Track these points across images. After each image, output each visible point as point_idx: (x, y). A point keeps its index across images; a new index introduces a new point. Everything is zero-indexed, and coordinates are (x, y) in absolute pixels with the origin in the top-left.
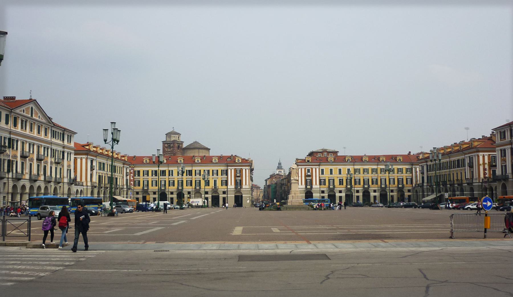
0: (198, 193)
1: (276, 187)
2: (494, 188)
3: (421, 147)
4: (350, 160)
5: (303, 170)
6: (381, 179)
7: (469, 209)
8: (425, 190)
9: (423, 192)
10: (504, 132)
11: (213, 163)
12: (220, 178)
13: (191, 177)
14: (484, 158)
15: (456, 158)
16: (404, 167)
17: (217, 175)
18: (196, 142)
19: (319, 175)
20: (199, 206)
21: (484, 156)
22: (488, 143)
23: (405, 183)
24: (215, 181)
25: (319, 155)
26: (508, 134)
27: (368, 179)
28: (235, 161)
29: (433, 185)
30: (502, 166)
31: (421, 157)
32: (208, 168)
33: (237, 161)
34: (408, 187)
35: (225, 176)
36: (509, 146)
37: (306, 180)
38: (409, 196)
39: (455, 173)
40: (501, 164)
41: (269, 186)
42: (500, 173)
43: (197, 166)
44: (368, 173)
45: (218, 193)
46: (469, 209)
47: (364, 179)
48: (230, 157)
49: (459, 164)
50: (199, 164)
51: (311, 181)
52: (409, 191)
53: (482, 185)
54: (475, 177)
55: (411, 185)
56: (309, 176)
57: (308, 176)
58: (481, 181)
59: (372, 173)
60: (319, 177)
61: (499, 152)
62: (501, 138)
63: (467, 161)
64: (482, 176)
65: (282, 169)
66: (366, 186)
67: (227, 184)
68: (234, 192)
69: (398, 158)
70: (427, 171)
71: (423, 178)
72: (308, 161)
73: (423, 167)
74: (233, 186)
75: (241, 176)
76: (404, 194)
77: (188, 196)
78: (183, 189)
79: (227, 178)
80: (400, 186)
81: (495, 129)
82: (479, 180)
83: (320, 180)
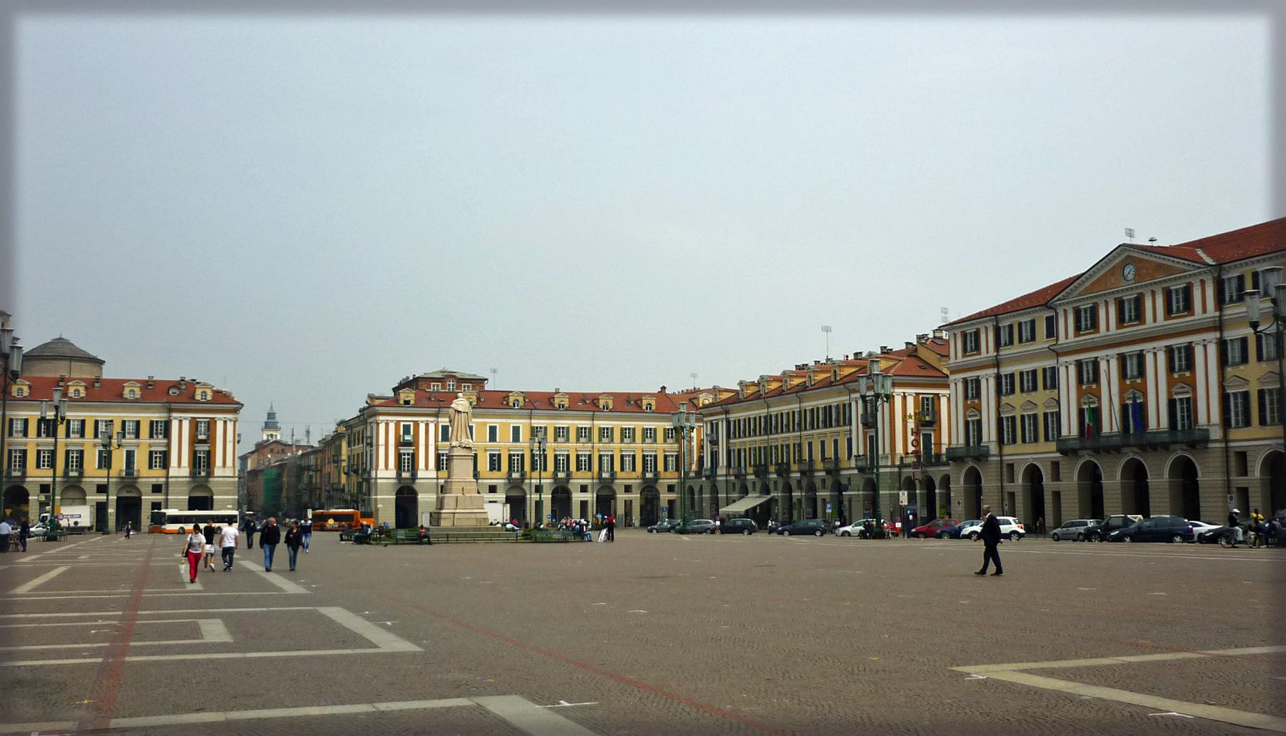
0: (74, 490)
1: (280, 476)
2: (937, 483)
3: (694, 376)
4: (521, 404)
5: (392, 426)
6: (600, 457)
7: (1014, 538)
8: (722, 487)
9: (714, 490)
10: (977, 334)
11: (126, 401)
12: (143, 447)
13: (52, 440)
14: (905, 401)
15: (822, 403)
16: (661, 426)
17: (137, 436)
18: (60, 340)
19: (436, 441)
20: (83, 529)
21: (904, 397)
22: (919, 361)
23: (660, 467)
24: (130, 455)
25: (435, 387)
26: (987, 340)
27: (568, 456)
28: (193, 397)
29: (746, 474)
30: (967, 424)
31: (705, 399)
32: (103, 416)
33: (198, 397)
34: (669, 477)
35: (161, 440)
36: (993, 371)
37: (399, 457)
38: (671, 502)
39: (818, 441)
40: (965, 416)
41: (254, 473)
42: (962, 441)
43: (77, 409)
44: (568, 440)
45: (209, 490)
46: (1014, 538)
47: (556, 456)
48: (176, 385)
49: (832, 417)
50: (78, 402)
51: (414, 457)
52: (671, 488)
53: (900, 473)
54: (881, 452)
55: (676, 474)
56: (408, 444)
57: (406, 443)
58: (898, 463)
59: (578, 441)
60: (437, 449)
61: (960, 386)
62: (965, 350)
63: (857, 410)
64: (899, 449)
65: (276, 428)
66: (561, 475)
67: (165, 464)
68: (186, 489)
69: (645, 402)
70: (728, 437)
71: (714, 455)
72: (407, 402)
73: (714, 427)
74: (185, 471)
75: (210, 440)
76: (658, 498)
77: (42, 498)
78: (24, 475)
79: (169, 445)
80: (649, 475)
81: (950, 326)
82: (893, 461)
83: (438, 456)
